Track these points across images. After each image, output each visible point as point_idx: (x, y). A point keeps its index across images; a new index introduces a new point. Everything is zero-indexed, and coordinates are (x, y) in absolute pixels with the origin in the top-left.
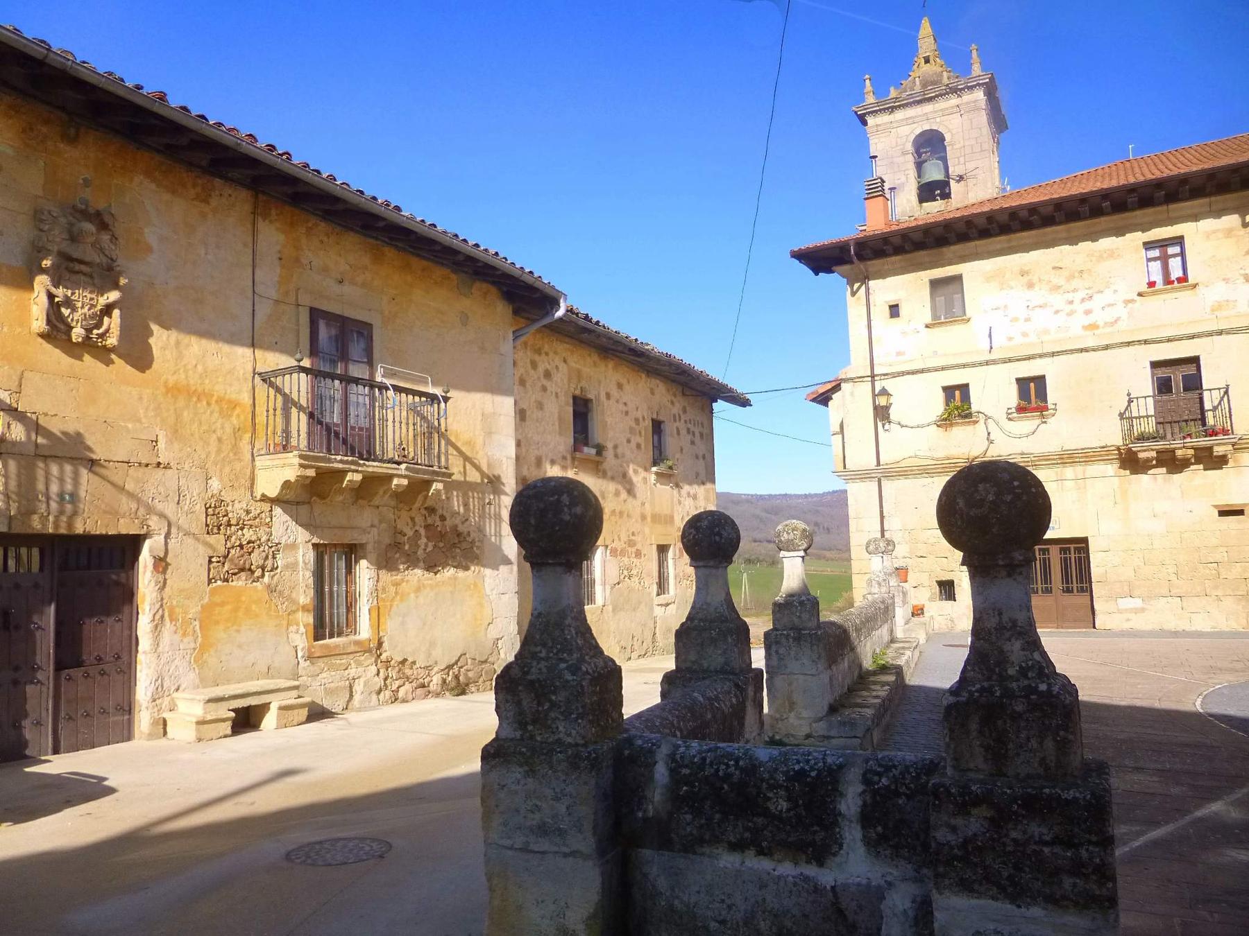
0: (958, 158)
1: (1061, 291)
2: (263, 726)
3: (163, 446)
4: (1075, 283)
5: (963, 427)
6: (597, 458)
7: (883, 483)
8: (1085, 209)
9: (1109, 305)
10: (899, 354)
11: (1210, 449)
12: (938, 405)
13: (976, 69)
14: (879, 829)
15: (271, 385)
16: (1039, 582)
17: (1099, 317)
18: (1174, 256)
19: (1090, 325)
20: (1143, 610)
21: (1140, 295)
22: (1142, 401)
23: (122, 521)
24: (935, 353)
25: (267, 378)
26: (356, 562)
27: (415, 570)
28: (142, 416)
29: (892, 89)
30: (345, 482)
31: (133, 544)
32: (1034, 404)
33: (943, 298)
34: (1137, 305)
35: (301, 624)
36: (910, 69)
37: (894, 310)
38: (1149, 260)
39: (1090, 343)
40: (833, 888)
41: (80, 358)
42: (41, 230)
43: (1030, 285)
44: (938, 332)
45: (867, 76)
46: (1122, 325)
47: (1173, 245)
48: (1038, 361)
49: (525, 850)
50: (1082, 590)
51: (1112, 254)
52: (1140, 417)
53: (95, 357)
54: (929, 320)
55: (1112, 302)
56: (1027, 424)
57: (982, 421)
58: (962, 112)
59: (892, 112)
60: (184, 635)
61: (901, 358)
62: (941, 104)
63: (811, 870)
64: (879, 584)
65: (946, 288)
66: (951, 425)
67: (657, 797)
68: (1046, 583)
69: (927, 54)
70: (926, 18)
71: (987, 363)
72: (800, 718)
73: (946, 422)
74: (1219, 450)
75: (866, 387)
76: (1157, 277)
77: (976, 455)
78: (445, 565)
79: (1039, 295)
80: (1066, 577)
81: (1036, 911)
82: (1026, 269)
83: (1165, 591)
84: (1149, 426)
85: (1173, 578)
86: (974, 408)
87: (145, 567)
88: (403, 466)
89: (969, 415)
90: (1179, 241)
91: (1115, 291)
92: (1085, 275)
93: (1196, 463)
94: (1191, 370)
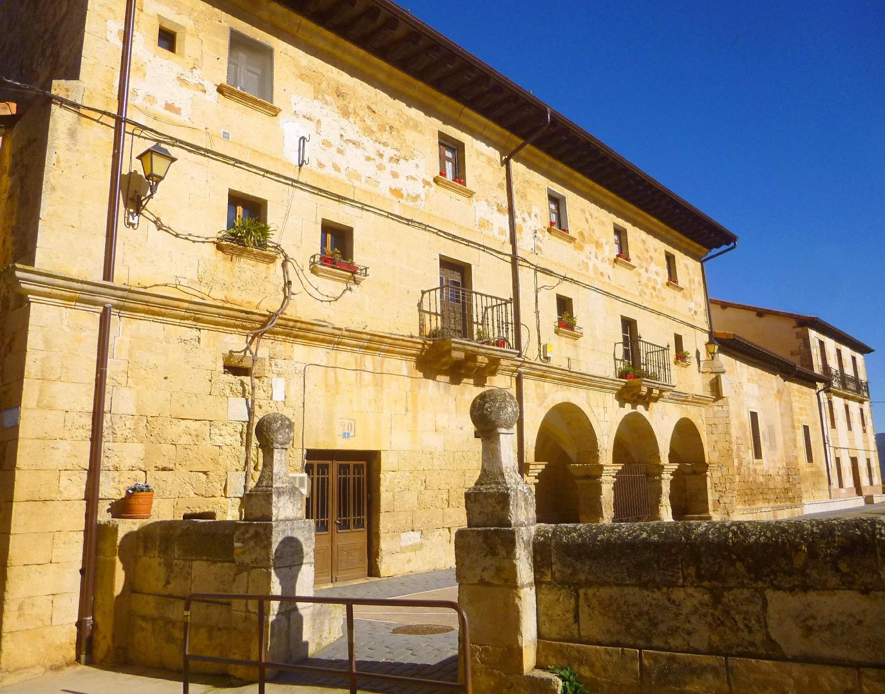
2: (159, 47)
4: (385, 137)
7: (114, 319)
9: (412, 178)
10: (169, 107)
17: (401, 183)
20: (421, 546)
24: (226, 136)
34: (433, 189)
46: (421, 204)
50: (358, 524)
51: (416, 126)
52: (430, 313)
54: (223, 79)
55: (415, 177)
61: (174, 116)
79: (352, 130)
80: (343, 510)
92: (394, 133)
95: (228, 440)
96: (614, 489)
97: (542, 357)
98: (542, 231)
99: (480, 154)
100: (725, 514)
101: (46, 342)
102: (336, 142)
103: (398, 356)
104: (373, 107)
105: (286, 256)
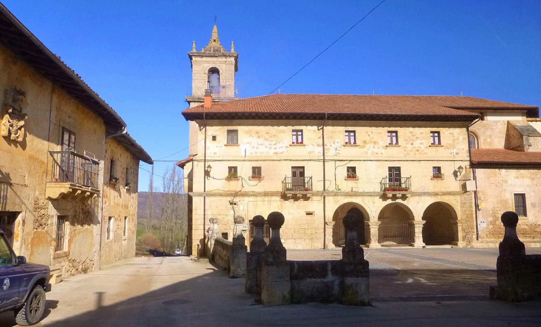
0: (224, 80)
1: (268, 140)
3: (27, 178)
4: (272, 139)
5: (234, 181)
6: (115, 183)
7: (206, 198)
8: (278, 117)
9: (281, 147)
10: (215, 153)
11: (306, 195)
12: (226, 174)
13: (233, 50)
14: (334, 271)
15: (52, 156)
16: (265, 234)
17: (278, 150)
18: (300, 135)
19: (275, 153)
21: (290, 145)
22: (289, 178)
23: (16, 206)
25: (51, 153)
26: (63, 223)
27: (79, 226)
28: (23, 167)
29: (203, 49)
30: (77, 194)
31: (14, 215)
32: (257, 176)
33: (231, 136)
34: (289, 148)
35: (53, 245)
36: (208, 42)
37: (214, 138)
38: (293, 135)
39: (275, 158)
40: (326, 282)
41: (10, 145)
42: (6, 97)
43: (259, 137)
44: (228, 147)
45: (194, 42)
46: (284, 154)
47: (300, 132)
48: (259, 162)
49: (276, 281)
51: (283, 132)
52: (288, 183)
53: (61, 155)
56: (254, 182)
57: (241, 180)
58: (227, 64)
59: (202, 57)
60: (27, 250)
62: (219, 59)
63: (323, 280)
64: (217, 233)
65: (232, 134)
66: (231, 180)
67: (296, 270)
68: (252, 235)
69: (215, 39)
70: (215, 25)
71: (244, 161)
72: (241, 270)
73: (229, 179)
74: (308, 195)
75: (203, 163)
76: (295, 141)
77: (238, 191)
78: (85, 224)
79: (261, 141)
81: (360, 278)
82: (258, 131)
83: (291, 237)
84: (289, 186)
85: (293, 233)
86: (238, 175)
87: (19, 224)
88: (90, 188)
89: (237, 177)
90: (302, 131)
91: (283, 143)
93: (302, 199)
94: (302, 170)
95: (230, 219)
96: (379, 230)
97: (337, 189)
98: (340, 147)
99: (309, 131)
100: (468, 242)
101: (196, 204)
102: (256, 146)
103: (276, 196)
104: (268, 132)
105: (242, 178)
